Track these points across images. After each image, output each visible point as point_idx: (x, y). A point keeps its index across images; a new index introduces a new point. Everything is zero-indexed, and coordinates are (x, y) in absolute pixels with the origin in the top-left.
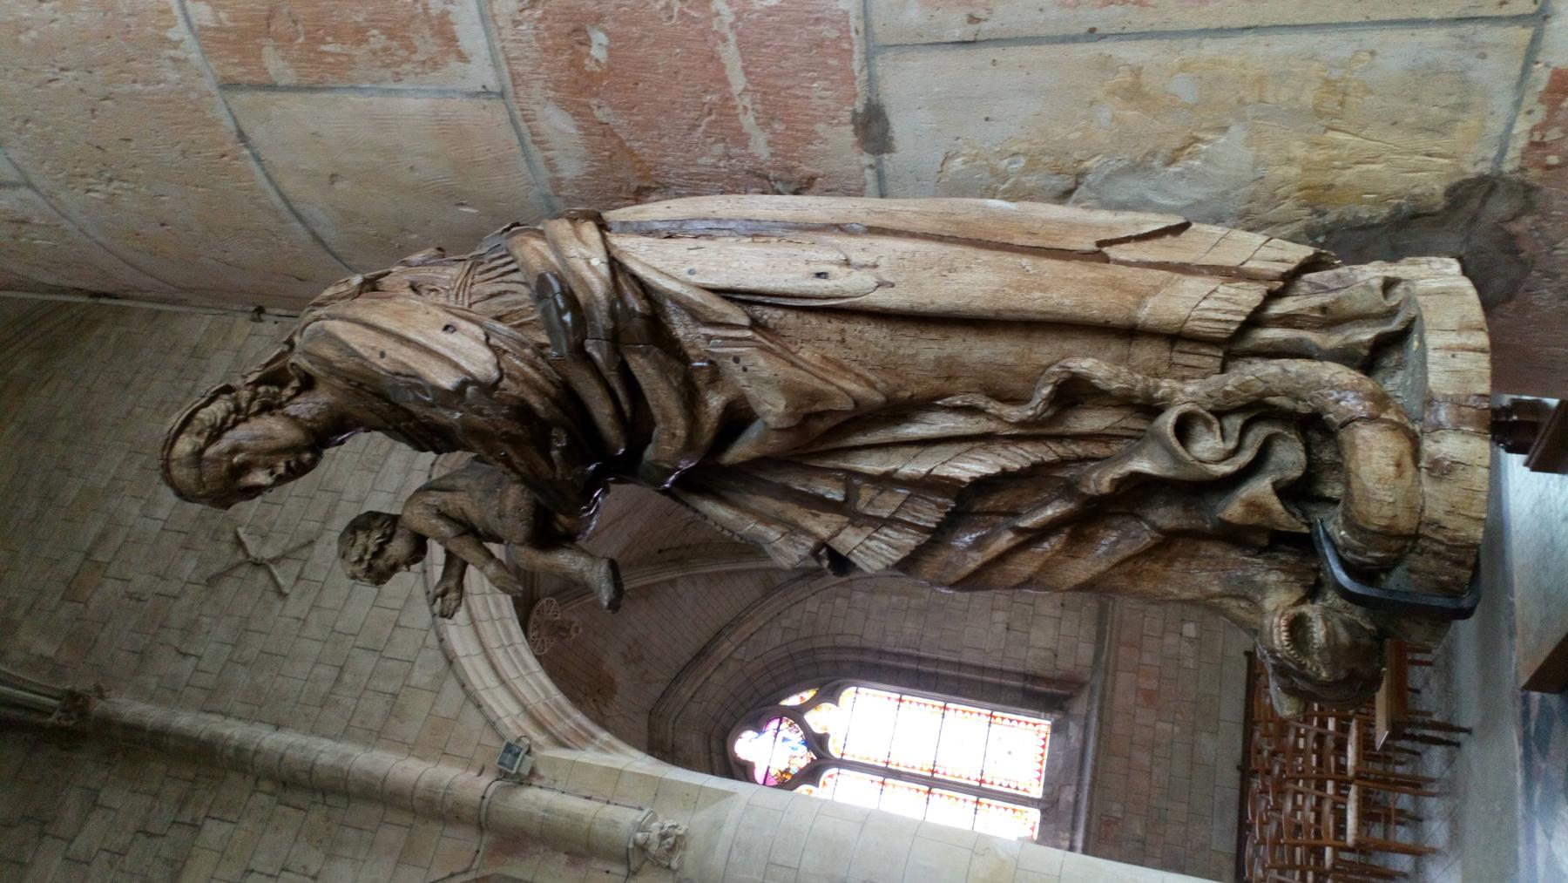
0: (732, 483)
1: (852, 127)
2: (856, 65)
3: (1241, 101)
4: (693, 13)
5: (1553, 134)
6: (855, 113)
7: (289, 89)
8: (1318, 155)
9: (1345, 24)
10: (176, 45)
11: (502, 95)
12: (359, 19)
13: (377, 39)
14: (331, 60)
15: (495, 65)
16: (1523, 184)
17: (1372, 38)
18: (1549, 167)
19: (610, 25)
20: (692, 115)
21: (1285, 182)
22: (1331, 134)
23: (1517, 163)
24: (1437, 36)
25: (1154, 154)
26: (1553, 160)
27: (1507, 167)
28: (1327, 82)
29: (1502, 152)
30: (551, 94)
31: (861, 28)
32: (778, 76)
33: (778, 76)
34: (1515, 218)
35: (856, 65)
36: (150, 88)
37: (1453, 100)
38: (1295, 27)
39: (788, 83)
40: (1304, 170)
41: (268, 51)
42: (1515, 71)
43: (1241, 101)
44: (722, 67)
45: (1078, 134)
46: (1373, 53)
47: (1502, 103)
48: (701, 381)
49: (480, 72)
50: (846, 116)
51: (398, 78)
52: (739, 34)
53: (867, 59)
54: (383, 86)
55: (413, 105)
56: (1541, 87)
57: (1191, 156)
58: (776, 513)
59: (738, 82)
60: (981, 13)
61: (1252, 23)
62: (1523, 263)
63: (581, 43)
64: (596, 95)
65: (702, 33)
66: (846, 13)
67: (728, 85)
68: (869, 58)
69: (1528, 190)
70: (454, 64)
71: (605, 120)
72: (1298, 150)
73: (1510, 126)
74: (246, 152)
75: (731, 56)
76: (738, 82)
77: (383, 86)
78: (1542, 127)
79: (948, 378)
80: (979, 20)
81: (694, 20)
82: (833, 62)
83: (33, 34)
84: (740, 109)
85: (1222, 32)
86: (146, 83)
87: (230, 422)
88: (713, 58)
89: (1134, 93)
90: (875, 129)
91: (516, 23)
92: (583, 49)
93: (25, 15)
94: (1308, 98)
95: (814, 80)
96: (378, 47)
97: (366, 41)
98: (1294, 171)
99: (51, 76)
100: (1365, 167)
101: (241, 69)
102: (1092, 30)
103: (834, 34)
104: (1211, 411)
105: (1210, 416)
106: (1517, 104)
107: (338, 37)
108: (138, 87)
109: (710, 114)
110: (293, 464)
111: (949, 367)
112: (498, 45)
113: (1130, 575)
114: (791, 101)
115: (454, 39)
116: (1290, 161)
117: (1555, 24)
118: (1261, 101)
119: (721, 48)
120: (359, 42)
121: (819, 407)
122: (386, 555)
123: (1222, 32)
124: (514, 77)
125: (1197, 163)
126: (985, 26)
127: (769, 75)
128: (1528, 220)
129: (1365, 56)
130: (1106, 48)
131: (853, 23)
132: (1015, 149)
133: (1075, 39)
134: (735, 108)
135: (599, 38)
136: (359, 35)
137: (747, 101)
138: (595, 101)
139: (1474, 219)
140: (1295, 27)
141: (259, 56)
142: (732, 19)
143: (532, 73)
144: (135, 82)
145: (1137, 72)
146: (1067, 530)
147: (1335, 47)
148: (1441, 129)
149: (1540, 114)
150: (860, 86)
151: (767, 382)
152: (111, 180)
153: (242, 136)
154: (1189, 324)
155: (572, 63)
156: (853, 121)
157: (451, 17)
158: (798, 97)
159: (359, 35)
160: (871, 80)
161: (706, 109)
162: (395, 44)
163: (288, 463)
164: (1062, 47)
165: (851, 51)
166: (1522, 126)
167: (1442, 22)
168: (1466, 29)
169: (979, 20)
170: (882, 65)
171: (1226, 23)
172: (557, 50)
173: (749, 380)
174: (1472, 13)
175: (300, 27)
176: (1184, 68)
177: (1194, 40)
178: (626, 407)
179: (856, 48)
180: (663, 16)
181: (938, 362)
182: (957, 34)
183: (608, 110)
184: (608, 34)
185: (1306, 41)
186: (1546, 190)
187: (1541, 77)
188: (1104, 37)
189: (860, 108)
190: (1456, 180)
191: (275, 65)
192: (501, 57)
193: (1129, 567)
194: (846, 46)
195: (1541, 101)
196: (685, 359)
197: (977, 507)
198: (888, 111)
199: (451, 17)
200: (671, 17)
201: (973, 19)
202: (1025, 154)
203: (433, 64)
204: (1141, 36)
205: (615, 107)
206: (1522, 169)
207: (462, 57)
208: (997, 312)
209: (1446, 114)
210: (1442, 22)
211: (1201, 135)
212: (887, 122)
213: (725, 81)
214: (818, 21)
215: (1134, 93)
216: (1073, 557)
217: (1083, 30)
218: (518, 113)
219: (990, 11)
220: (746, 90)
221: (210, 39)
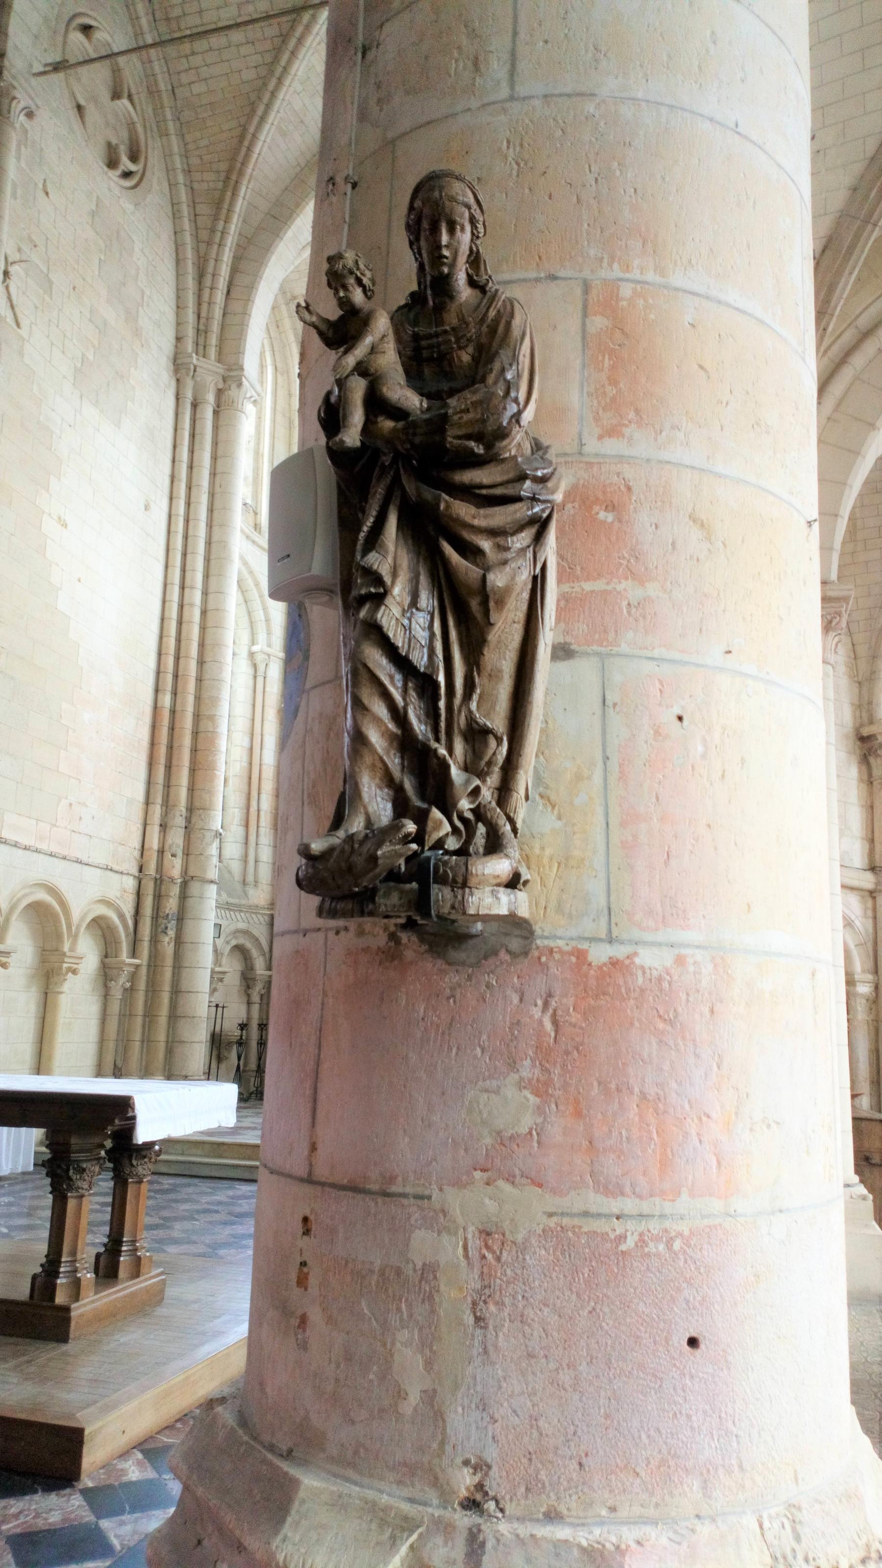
0: (410, 541)
1: (562, 641)
2: (595, 648)
3: (574, 825)
4: (621, 570)
5: (557, 956)
6: (570, 644)
7: (584, 324)
8: (545, 861)
9: (608, 864)
10: (610, 265)
11: (580, 453)
12: (622, 385)
13: (611, 391)
14: (600, 358)
15: (596, 455)
16: (530, 949)
17: (602, 875)
18: (539, 958)
19: (616, 525)
20: (569, 558)
21: (531, 848)
22: (556, 865)
23: (541, 945)
24: (603, 902)
25: (547, 788)
26: (543, 959)
27: (538, 942)
28: (583, 860)
29: (547, 938)
30: (581, 482)
31: (613, 652)
32: (590, 608)
33: (590, 608)
34: (508, 951)
35: (595, 648)
36: (585, 234)
37: (574, 913)
38: (608, 843)
39: (587, 613)
40: (538, 857)
41: (606, 322)
42: (586, 935)
43: (574, 825)
44: (594, 580)
45: (558, 752)
46: (596, 877)
47: (573, 932)
48: (500, 540)
49: (592, 446)
50: (569, 639)
51: (590, 394)
52: (611, 592)
53: (597, 653)
54: (585, 384)
55: (575, 398)
56: (579, 946)
57: (545, 805)
58: (400, 565)
59: (588, 586)
60: (617, 709)
61: (610, 827)
62: (479, 962)
63: (606, 507)
64: (580, 507)
65: (612, 573)
66: (619, 646)
67: (585, 581)
68: (598, 654)
69: (526, 954)
70: (597, 431)
71: (566, 508)
72: (548, 852)
73: (560, 938)
74: (542, 275)
75: (599, 585)
76: (588, 586)
77: (585, 384)
78: (561, 951)
79: (490, 675)
80: (614, 708)
81: (617, 570)
82: (597, 636)
83: (618, 173)
84: (572, 584)
85: (607, 814)
86: (588, 233)
87: (475, 232)
88: (600, 576)
89: (579, 778)
90: (561, 653)
91: (618, 474)
92: (604, 508)
93: (629, 175)
94: (576, 853)
95: (588, 626)
96: (607, 390)
97: (610, 384)
98: (537, 851)
99: (593, 169)
100: (539, 881)
101: (596, 299)
102: (608, 758)
103: (610, 639)
104: (480, 803)
105: (477, 803)
106: (572, 939)
107: (613, 367)
108: (586, 226)
109: (570, 568)
110: (445, 260)
111: (497, 677)
112: (607, 460)
113: (373, 766)
114: (577, 612)
115: (610, 436)
116: (543, 849)
117: (608, 946)
118: (574, 833)
119: (605, 581)
120: (609, 378)
121: (492, 604)
122: (356, 287)
123: (607, 814)
124: (591, 464)
125: (541, 808)
126: (611, 710)
127: (590, 602)
128: (508, 957)
129: (594, 874)
130: (600, 764)
131: (615, 649)
132: (550, 722)
133: (604, 750)
134: (573, 582)
135: (610, 517)
136: (614, 382)
137: (577, 589)
138: (576, 505)
139: (506, 934)
140: (608, 843)
141: (602, 315)
142: (618, 589)
143: (593, 476)
144: (589, 225)
145: (589, 778)
146: (399, 732)
147: (599, 861)
148: (559, 909)
149: (566, 949)
150: (584, 648)
151: (513, 578)
152: (518, 164)
153: (553, 278)
154: (515, 794)
155: (597, 499)
156: (566, 643)
157: (621, 438)
158: (579, 616)
159: (614, 382)
160: (587, 654)
161: (573, 567)
162: (608, 400)
163: (446, 258)
164: (600, 747)
165: (602, 646)
166: (560, 943)
167: (609, 903)
168: (606, 912)
169: (614, 708)
170: (594, 660)
171: (611, 815)
172: (604, 492)
173: (514, 569)
174: (612, 913)
175: (617, 347)
176: (591, 798)
177: (604, 803)
178: (484, 492)
179: (603, 649)
180: (620, 555)
181: (500, 671)
182: (608, 697)
183: (572, 512)
184: (612, 523)
185: (601, 847)
186: (526, 961)
187: (584, 946)
188: (605, 764)
189: (572, 647)
190: (532, 922)
191: (598, 323)
192: (601, 460)
193: (379, 765)
194: (605, 644)
195: (573, 948)
196: (513, 534)
197: (410, 685)
198: (571, 661)
199: (621, 438)
200: (619, 558)
201: (615, 705)
202: (547, 727)
203: (597, 419)
204: (605, 779)
205: (574, 516)
206: (538, 948)
207: (600, 437)
208: (531, 703)
209: (567, 911)
210: (609, 903)
211: (556, 808)
212: (564, 660)
213: (588, 579)
214: (616, 631)
215: (579, 778)
216: (383, 735)
217: (608, 754)
218: (570, 459)
219: (618, 713)
220: (583, 590)
221: (612, 286)
